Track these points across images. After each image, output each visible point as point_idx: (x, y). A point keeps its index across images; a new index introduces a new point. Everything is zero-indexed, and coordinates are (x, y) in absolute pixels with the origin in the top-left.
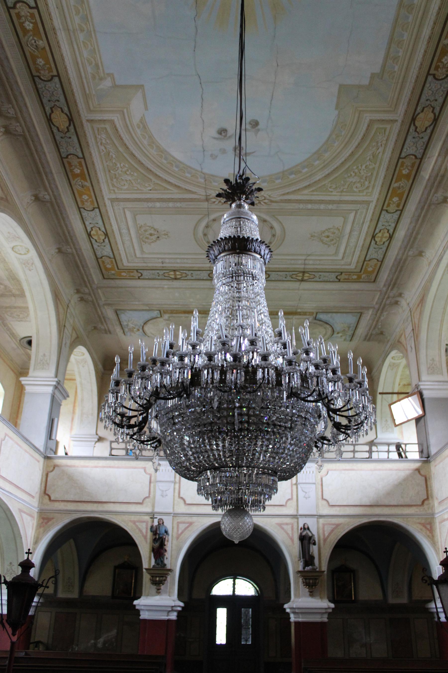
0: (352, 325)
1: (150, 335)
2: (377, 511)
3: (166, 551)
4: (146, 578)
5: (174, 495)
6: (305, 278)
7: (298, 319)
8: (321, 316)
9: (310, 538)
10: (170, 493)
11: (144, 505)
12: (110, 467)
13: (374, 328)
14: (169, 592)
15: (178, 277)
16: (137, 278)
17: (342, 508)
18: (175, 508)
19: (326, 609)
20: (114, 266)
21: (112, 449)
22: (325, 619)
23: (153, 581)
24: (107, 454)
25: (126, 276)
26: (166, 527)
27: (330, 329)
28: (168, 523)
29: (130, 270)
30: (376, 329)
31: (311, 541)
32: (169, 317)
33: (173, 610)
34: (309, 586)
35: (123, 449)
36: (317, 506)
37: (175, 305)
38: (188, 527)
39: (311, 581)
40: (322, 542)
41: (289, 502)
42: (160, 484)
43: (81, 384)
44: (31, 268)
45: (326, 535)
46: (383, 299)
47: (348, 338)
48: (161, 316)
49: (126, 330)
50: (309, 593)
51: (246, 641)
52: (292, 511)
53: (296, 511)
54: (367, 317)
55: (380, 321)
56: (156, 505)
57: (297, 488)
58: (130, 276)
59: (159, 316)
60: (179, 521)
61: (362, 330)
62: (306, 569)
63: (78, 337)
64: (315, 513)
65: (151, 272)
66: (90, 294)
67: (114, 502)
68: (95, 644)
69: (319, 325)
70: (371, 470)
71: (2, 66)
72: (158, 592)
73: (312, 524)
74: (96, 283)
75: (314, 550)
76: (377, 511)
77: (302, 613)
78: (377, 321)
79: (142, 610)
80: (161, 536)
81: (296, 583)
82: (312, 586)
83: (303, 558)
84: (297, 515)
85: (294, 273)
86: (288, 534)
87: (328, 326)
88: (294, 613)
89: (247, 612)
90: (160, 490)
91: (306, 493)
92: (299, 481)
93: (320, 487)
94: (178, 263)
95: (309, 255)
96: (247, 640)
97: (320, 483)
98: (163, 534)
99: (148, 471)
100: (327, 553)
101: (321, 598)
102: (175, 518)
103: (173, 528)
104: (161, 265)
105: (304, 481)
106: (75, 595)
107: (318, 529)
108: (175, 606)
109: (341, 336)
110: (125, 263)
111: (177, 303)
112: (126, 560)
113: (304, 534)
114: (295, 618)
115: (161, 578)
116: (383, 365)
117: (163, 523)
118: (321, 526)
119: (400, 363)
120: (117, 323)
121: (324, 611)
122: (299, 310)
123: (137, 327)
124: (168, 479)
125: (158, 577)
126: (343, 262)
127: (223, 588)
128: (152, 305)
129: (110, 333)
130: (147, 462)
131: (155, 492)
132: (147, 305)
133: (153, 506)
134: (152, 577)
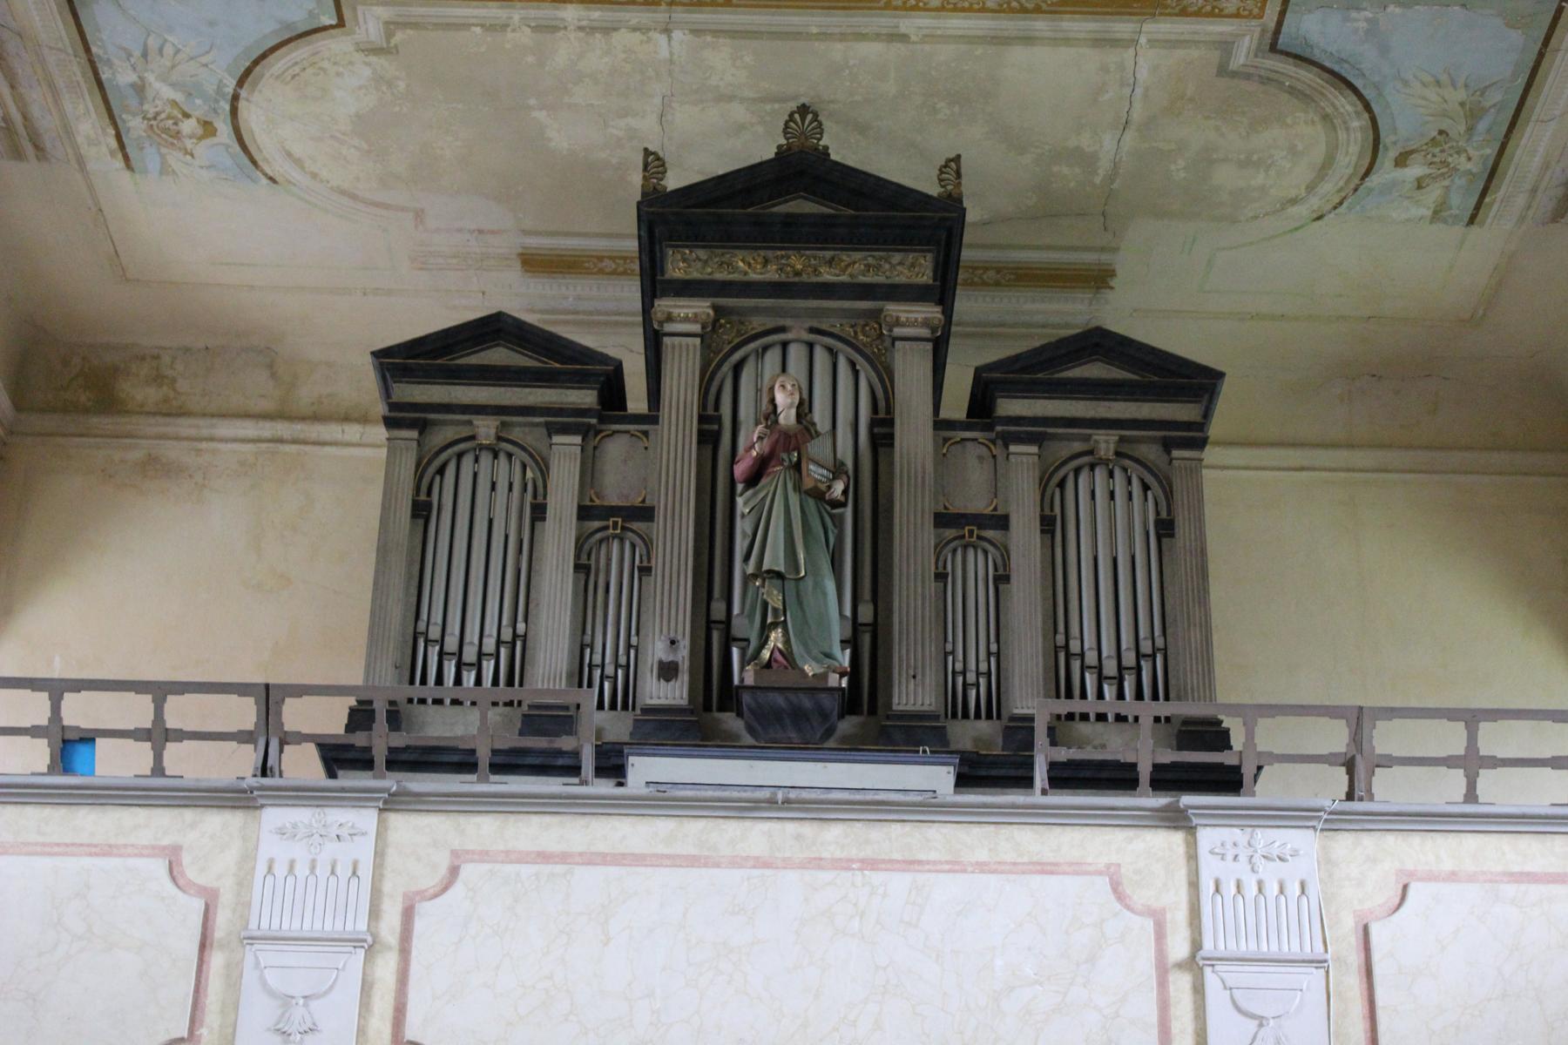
0: (1495, 97)
1: (279, 166)
27: (1359, 123)
32: (391, 27)
35: (34, 732)
42: (269, 955)
47: (1461, 202)
48: (341, 23)
49: (135, 126)
57: (1199, 990)
59: (329, 19)
69: (1292, 91)
87: (1345, 104)
90: (272, 993)
91: (1261, 1021)
92: (1208, 945)
93: (1352, 984)
97: (1355, 959)
99: (191, 873)
105: (1246, 947)
109: (1420, 185)
120: (76, 70)
123: (199, 108)
124: (330, 926)
130: (189, 814)
131: (232, 1005)
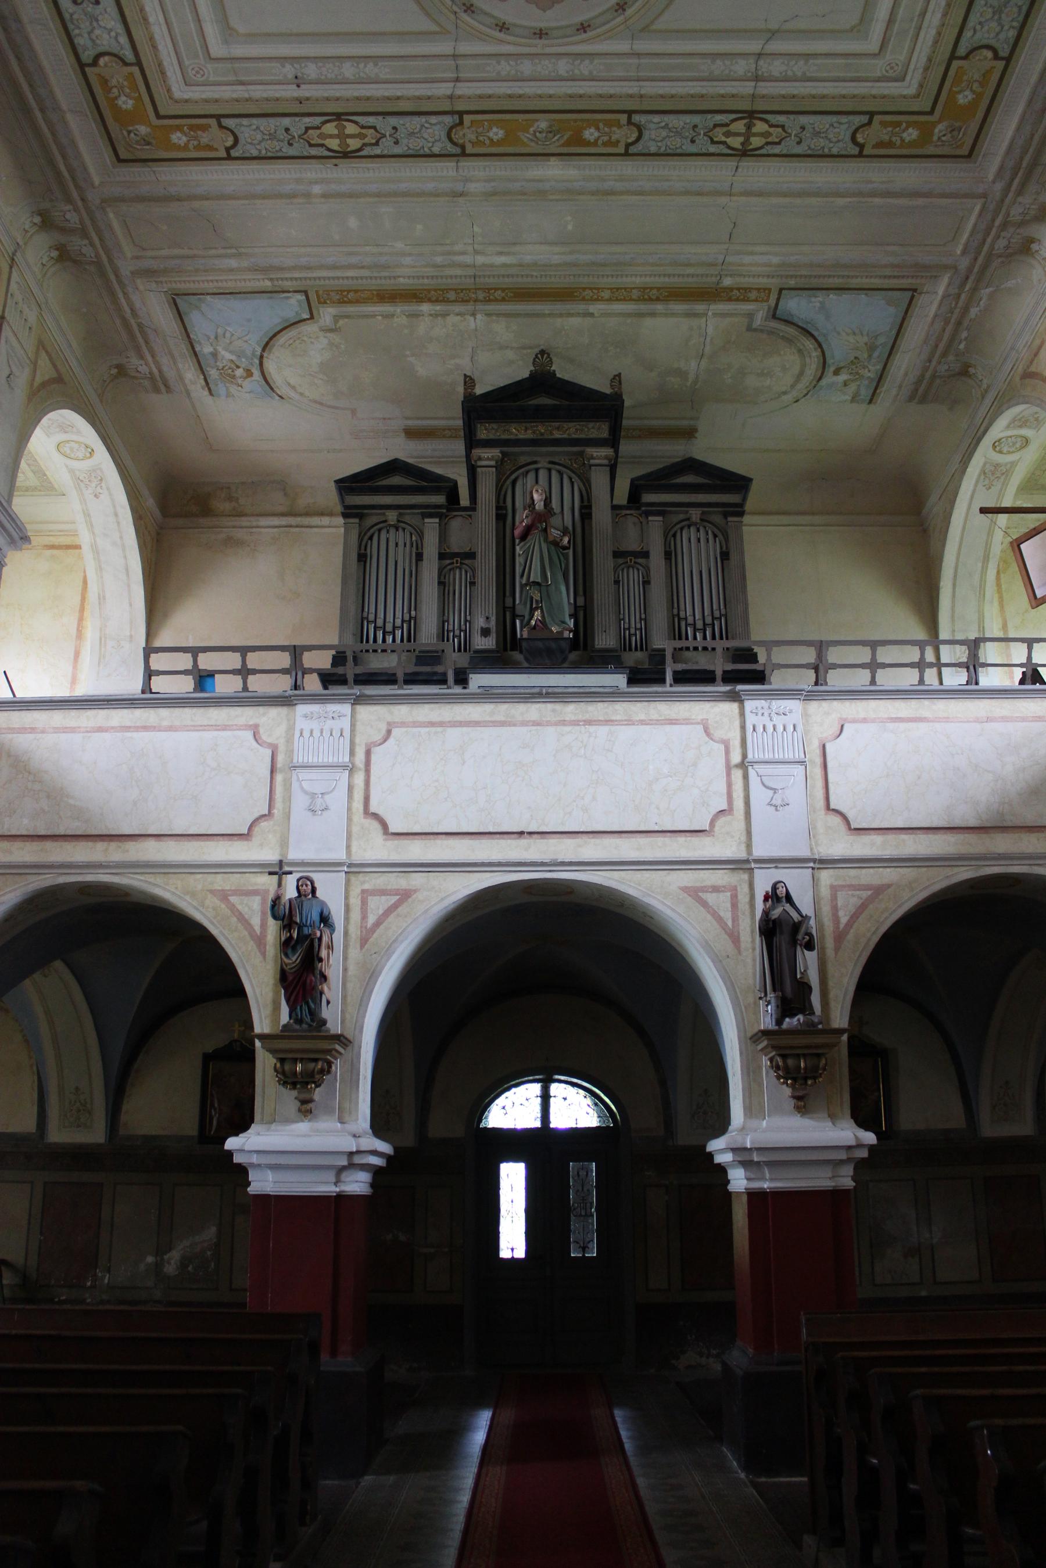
0: (881, 340)
1: (283, 390)
2: (1002, 844)
3: (324, 978)
4: (265, 1063)
5: (349, 809)
6: (756, 142)
7: (723, 315)
8: (796, 306)
9: (796, 927)
10: (338, 800)
11: (256, 839)
12: (145, 728)
13: (944, 354)
14: (341, 1110)
15: (354, 144)
16: (223, 154)
17: (890, 837)
18: (354, 849)
19: (849, 1148)
20: (140, 98)
21: (149, 674)
22: (846, 1180)
23: (284, 1073)
24: (134, 686)
25: (186, 148)
26: (323, 904)
28: (330, 891)
29: (196, 119)
30: (951, 358)
31: (800, 937)
32: (336, 318)
33: (351, 1166)
34: (795, 1079)
36: (811, 833)
37: (350, 267)
38: (395, 907)
39: (798, 1061)
40: (830, 944)
41: (721, 821)
42: (303, 774)
43: (96, 550)
44: (99, 490)
45: (844, 920)
46: (987, 233)
47: (865, 393)
48: (312, 317)
49: (213, 373)
50: (792, 1102)
51: (584, 1249)
52: (730, 848)
53: (743, 847)
54: (930, 305)
55: (966, 323)
56: (292, 840)
57: (746, 777)
58: (198, 148)
59: (306, 316)
60: (366, 886)
61: (906, 363)
62: (785, 1026)
63: (59, 380)
64: (805, 853)
65: (262, 122)
66: (85, 234)
67: (158, 836)
68: (158, 1266)
70: (977, 720)
71: (5, 30)
72: (306, 1109)
73: (798, 884)
74: (97, 181)
75: (808, 962)
76: (1002, 844)
77: (770, 1164)
78: (959, 323)
79: (252, 1165)
80: (306, 931)
81: (750, 1070)
82: (806, 1079)
83: (774, 990)
84: (747, 861)
85: (719, 118)
86: (719, 920)
87: (809, 344)
88: (746, 1164)
89: (583, 1173)
90: (306, 792)
91: (775, 790)
92: (750, 756)
93: (818, 771)
94: (345, 82)
95: (773, 34)
96: (585, 1244)
97: (819, 760)
98: (312, 925)
99: (264, 737)
100: (845, 979)
101: (833, 1117)
102: (353, 878)
103: (347, 909)
104: (291, 91)
105: (768, 756)
106: (95, 1134)
107: (816, 902)
108: (358, 1152)
109: (845, 384)
110: (179, 91)
111: (354, 260)
112: (236, 1036)
113: (776, 913)
114: (748, 1179)
115: (312, 1065)
116: (964, 472)
117: (314, 890)
118: (825, 892)
119: (1013, 464)
120: (184, 347)
121: (843, 1155)
122: (727, 282)
123: (244, 362)
125: (302, 1060)
126: (879, 67)
127: (514, 1109)
128: (281, 269)
129: (168, 389)
131: (288, 799)
132: (265, 270)
133: (284, 843)
134: (282, 1061)
